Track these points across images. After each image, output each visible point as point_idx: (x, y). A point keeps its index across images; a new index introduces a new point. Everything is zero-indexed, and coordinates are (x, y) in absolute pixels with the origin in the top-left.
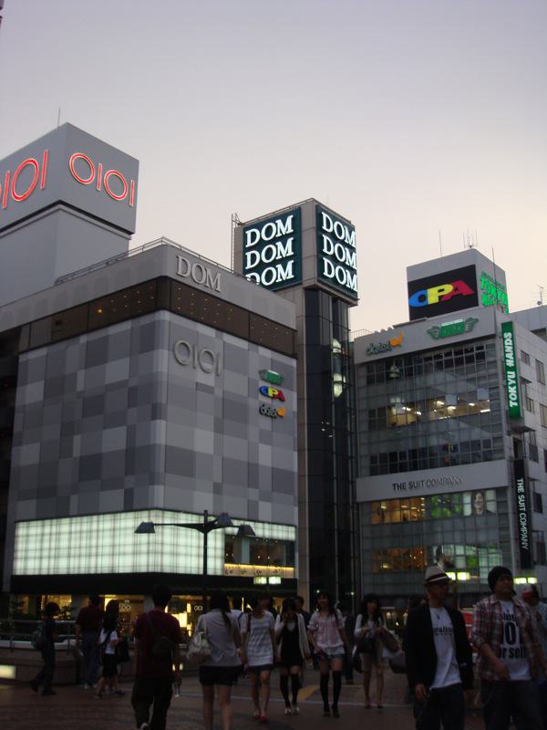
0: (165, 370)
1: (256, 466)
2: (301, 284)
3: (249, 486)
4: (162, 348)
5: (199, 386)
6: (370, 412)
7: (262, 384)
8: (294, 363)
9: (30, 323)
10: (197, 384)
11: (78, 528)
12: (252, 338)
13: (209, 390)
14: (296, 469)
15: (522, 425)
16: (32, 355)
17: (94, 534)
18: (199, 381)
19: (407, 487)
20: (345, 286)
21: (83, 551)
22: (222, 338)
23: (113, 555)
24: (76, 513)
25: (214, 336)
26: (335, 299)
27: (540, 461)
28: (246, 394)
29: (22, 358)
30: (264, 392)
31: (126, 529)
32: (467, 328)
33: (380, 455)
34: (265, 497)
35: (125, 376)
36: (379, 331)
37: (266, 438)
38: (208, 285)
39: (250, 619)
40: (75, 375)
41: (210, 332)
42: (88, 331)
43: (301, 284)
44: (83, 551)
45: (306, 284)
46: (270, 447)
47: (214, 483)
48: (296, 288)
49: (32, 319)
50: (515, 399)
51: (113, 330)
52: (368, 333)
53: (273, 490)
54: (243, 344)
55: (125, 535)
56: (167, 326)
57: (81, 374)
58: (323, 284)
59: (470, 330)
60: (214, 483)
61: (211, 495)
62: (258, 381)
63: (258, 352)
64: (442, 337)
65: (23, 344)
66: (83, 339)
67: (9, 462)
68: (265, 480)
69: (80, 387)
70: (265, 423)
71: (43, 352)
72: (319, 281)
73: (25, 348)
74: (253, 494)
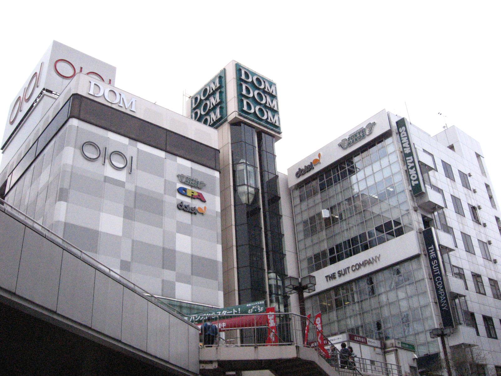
1: (174, 251)
3: (163, 268)
5: (107, 179)
6: (308, 260)
7: (179, 185)
8: (217, 174)
10: (105, 177)
13: (121, 184)
14: (219, 257)
15: (426, 201)
19: (337, 275)
20: (266, 121)
22: (136, 146)
26: (260, 133)
27: (470, 275)
28: (162, 191)
30: (182, 191)
32: (367, 133)
33: (315, 255)
34: (182, 278)
36: (333, 279)
37: (183, 229)
39: (166, 148)
46: (190, 286)
47: (122, 261)
50: (416, 178)
53: (192, 274)
54: (162, 154)
59: (370, 133)
60: (122, 261)
61: (122, 219)
62: (176, 184)
63: (176, 197)
64: (350, 145)
68: (184, 266)
70: (185, 217)
74: (169, 275)
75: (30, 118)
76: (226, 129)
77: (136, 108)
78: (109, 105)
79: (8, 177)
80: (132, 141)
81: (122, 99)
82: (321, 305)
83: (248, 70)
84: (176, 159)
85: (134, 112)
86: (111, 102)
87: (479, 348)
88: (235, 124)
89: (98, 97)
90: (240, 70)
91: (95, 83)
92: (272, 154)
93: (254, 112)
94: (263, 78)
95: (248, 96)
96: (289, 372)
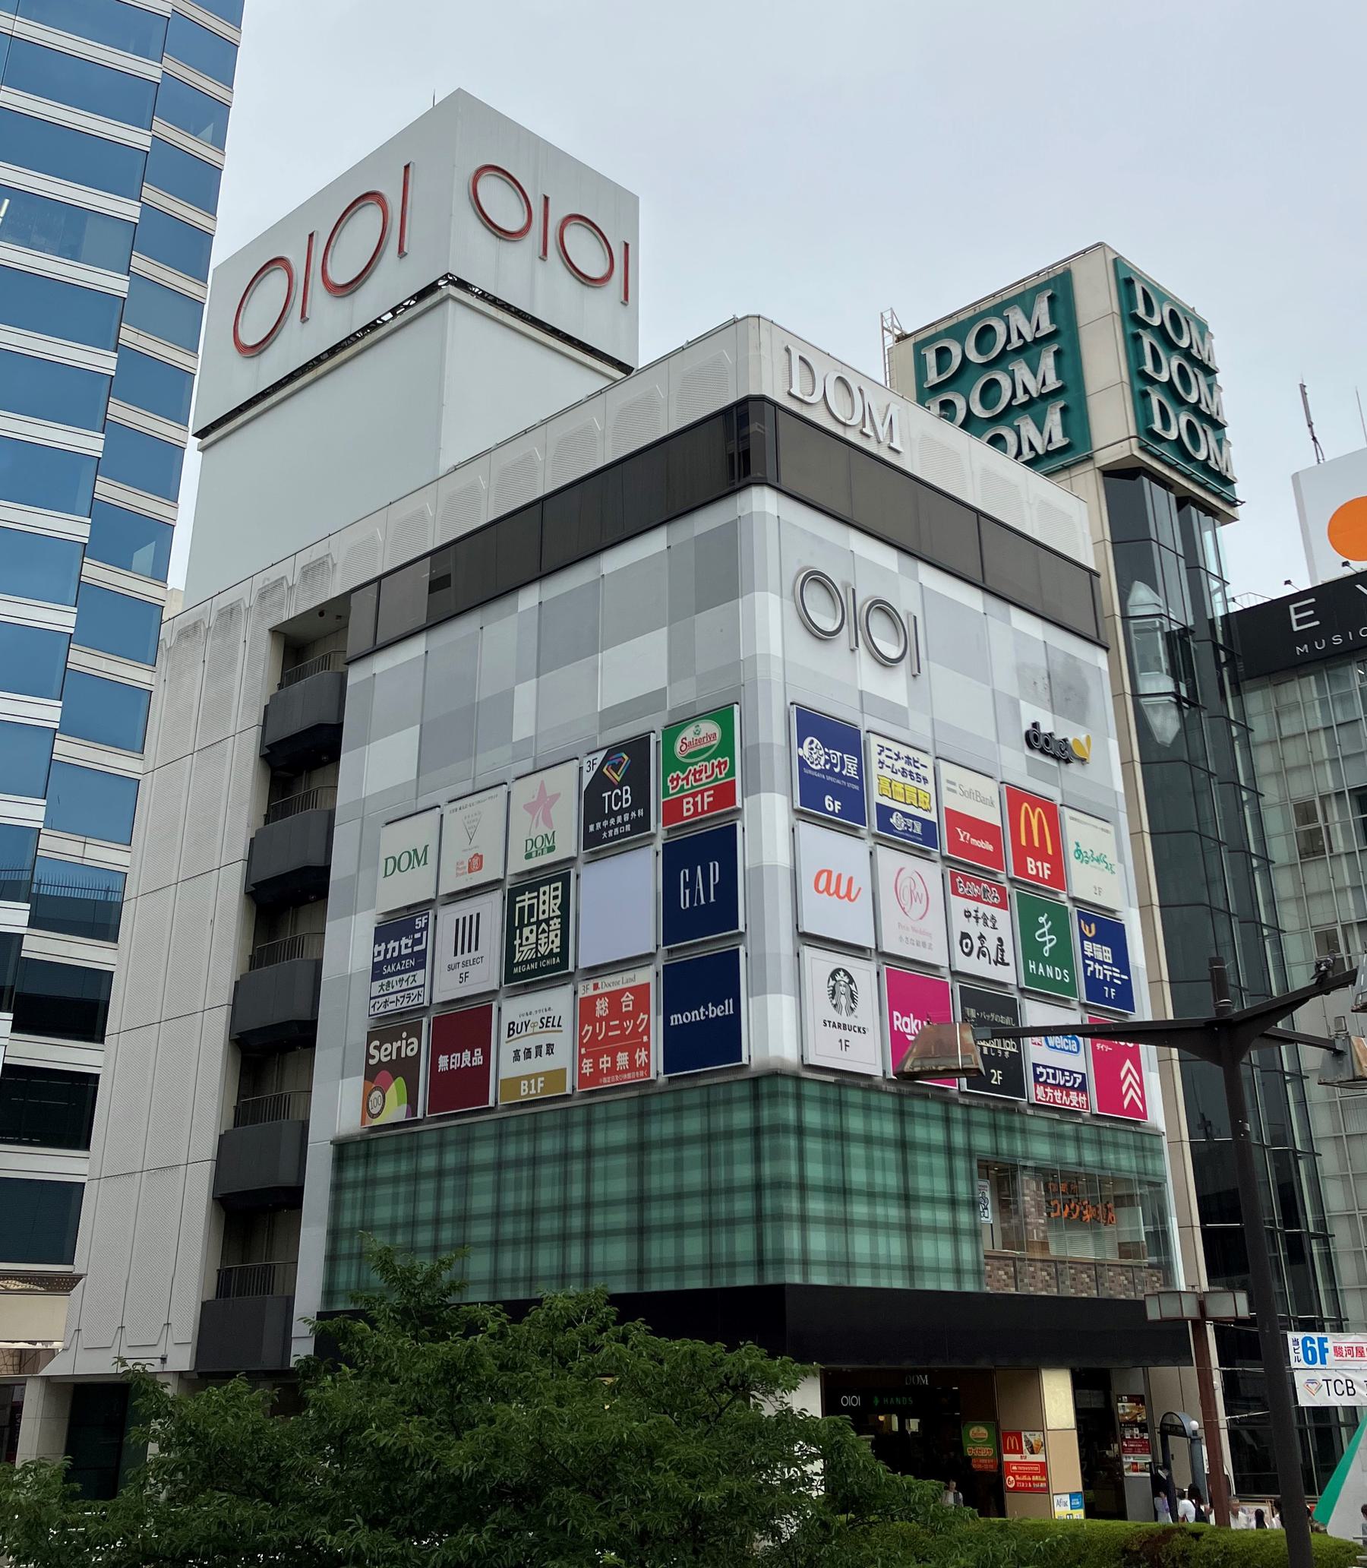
0: (775, 648)
2: (1090, 458)
4: (765, 589)
8: (1101, 659)
9: (378, 579)
11: (661, 1250)
12: (990, 584)
16: (382, 663)
17: (577, 1167)
18: (866, 689)
21: (548, 1225)
23: (501, 1136)
24: (422, 621)
25: (895, 569)
29: (356, 675)
31: (679, 1142)
35: (659, 680)
38: (867, 430)
40: (508, 696)
41: (887, 558)
42: (542, 575)
43: (1090, 458)
44: (548, 1225)
45: (1106, 457)
48: (1076, 471)
49: (379, 573)
51: (613, 562)
52: (1261, 601)
54: (972, 598)
55: (826, 1160)
56: (771, 527)
57: (525, 695)
58: (1157, 458)
65: (358, 635)
66: (529, 599)
67: (318, 965)
69: (523, 727)
71: (416, 648)
72: (1142, 449)
73: (367, 645)
75: (274, 344)
76: (1088, 481)
77: (902, 443)
78: (838, 430)
79: (1102, 829)
80: (908, 561)
81: (796, 362)
82: (1321, 962)
83: (1152, 287)
84: (1009, 612)
85: (897, 452)
86: (843, 420)
87: (402, 1189)
88: (1122, 475)
89: (850, 426)
90: (1129, 283)
91: (802, 355)
92: (887, 330)
93: (1175, 440)
94: (1185, 312)
95: (1156, 377)
96: (492, 1388)
